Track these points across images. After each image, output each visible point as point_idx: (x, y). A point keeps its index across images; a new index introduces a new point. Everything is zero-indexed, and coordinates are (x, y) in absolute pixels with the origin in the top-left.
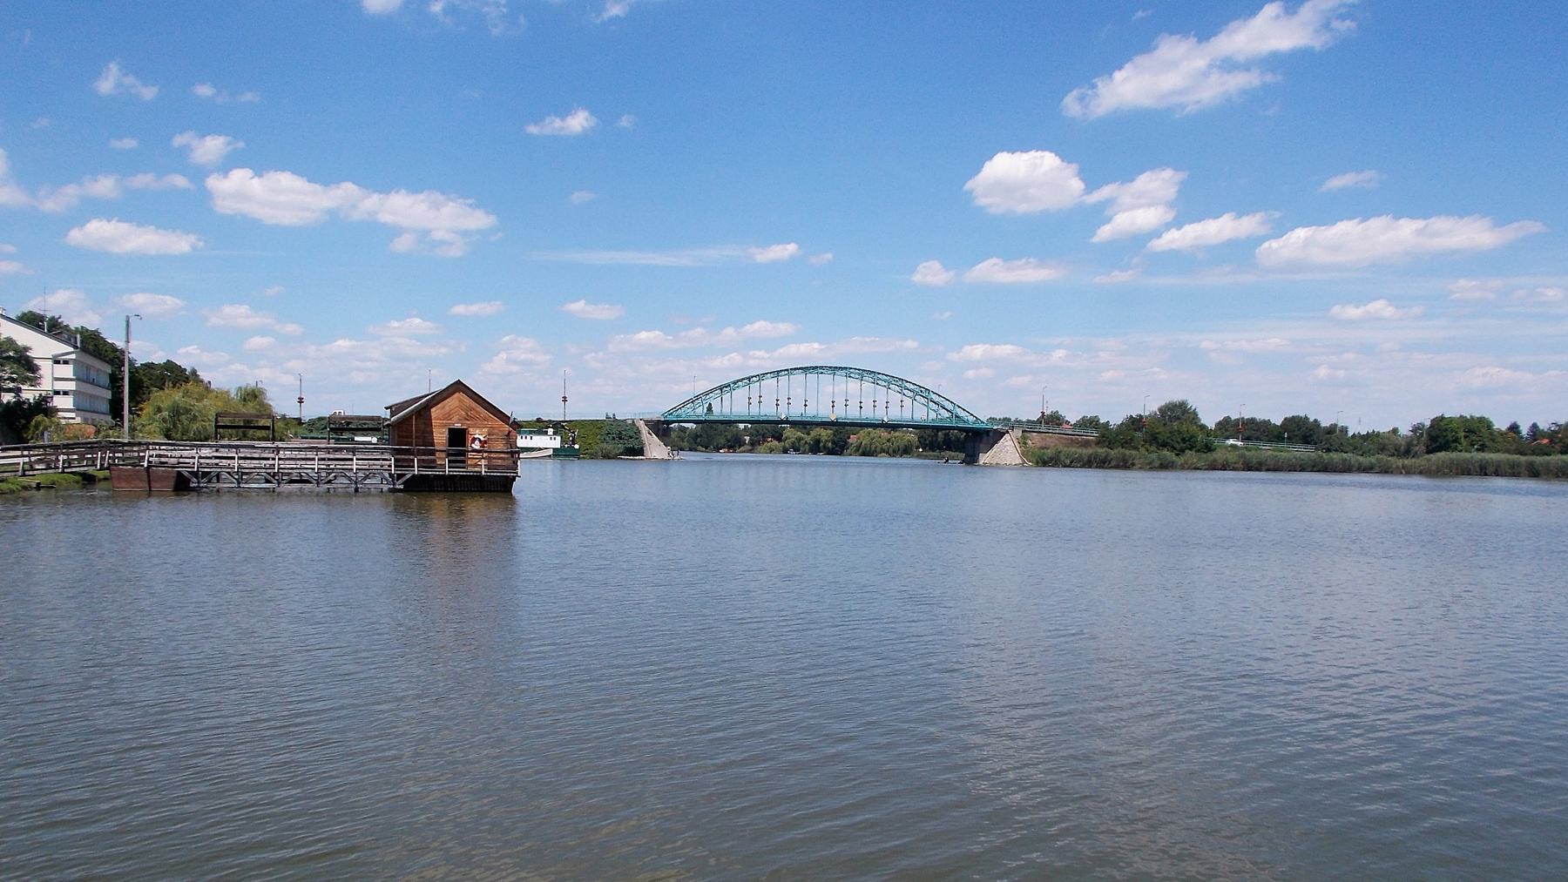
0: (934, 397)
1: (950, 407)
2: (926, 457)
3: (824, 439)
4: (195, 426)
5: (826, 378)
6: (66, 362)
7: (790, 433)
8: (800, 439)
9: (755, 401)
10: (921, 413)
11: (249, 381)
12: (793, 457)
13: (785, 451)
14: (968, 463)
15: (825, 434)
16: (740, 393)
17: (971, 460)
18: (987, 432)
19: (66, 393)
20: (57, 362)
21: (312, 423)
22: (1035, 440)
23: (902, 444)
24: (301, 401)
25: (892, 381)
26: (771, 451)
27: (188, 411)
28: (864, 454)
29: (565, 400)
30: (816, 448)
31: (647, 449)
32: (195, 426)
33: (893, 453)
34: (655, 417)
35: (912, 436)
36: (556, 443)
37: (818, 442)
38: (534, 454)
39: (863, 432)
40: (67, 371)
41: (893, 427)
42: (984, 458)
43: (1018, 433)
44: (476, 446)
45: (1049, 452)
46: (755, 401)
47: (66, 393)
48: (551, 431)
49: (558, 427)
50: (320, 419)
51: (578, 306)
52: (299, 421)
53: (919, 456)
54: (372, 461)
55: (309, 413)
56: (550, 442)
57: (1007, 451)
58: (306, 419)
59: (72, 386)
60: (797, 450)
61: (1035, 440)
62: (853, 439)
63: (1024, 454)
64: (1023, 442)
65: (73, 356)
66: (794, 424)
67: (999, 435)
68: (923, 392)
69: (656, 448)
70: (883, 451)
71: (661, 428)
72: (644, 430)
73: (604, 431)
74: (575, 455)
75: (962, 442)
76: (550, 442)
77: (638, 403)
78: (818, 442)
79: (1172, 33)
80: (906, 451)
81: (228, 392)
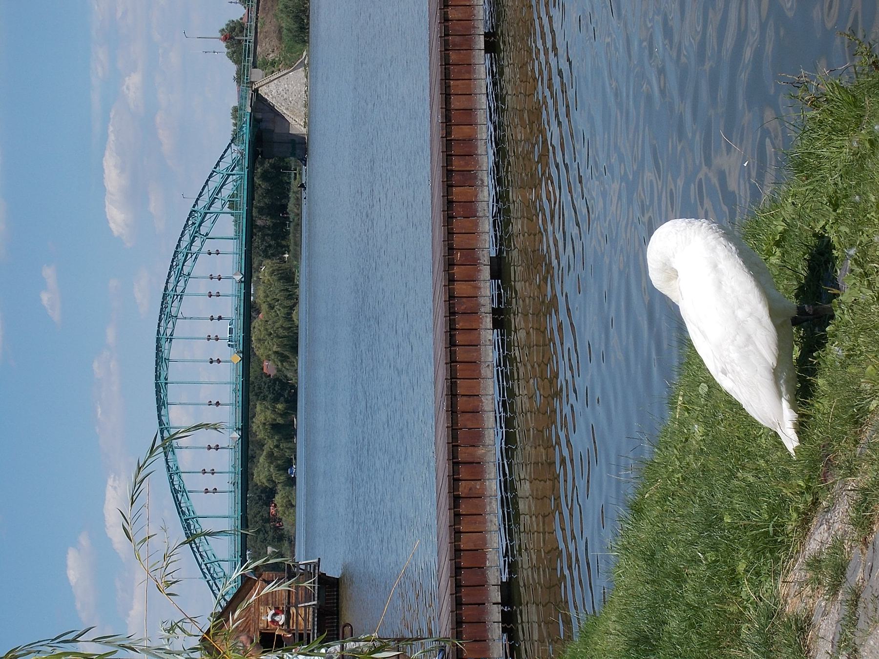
0: (202, 203)
1: (217, 180)
2: (298, 244)
5: (173, 372)
7: (262, 473)
8: (270, 455)
9: (211, 481)
10: (226, 228)
12: (299, 470)
13: (291, 482)
14: (305, 151)
15: (263, 415)
16: (198, 504)
17: (299, 147)
18: (256, 122)
22: (268, 48)
25: (177, 268)
26: (291, 505)
28: (294, 349)
30: (285, 430)
33: (292, 298)
35: (265, 270)
37: (275, 428)
39: (259, 351)
41: (249, 310)
42: (297, 127)
43: (257, 75)
44: (281, 619)
45: (287, 23)
46: (211, 481)
53: (297, 256)
57: (285, 91)
60: (289, 463)
61: (268, 48)
62: (270, 368)
63: (290, 65)
64: (270, 67)
66: (247, 459)
67: (260, 104)
68: (195, 223)
70: (288, 317)
78: (275, 428)
80: (288, 278)
81: (475, 73)
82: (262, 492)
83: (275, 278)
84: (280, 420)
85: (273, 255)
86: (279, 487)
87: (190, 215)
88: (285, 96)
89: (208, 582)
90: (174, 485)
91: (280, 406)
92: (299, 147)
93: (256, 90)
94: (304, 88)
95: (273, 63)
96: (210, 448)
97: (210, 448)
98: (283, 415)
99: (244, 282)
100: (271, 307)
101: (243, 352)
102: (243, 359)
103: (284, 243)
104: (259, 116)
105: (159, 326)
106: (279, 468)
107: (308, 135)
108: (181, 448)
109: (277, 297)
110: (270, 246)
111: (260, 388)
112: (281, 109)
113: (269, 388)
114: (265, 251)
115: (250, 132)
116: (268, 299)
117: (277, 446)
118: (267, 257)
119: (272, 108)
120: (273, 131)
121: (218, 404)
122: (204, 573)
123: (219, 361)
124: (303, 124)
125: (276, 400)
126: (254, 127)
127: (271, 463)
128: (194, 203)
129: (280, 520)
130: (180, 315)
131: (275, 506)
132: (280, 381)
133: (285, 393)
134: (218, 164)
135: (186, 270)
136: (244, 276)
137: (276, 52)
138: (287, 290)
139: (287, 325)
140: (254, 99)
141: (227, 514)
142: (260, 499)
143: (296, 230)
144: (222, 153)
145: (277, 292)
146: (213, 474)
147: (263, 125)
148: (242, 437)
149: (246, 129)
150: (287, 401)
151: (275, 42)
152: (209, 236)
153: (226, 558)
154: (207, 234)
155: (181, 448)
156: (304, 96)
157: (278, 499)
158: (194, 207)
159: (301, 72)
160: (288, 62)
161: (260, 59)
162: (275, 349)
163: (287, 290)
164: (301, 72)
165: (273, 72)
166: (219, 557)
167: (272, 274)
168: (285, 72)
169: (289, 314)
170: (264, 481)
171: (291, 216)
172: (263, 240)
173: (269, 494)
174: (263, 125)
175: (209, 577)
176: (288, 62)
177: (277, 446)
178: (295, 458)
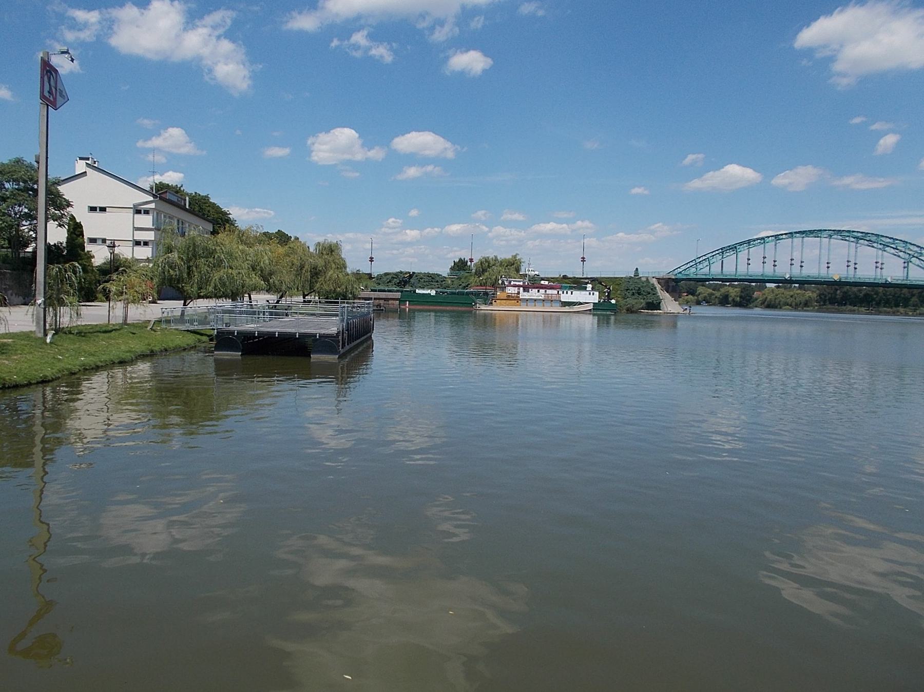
3: (733, 295)
4: (216, 276)
6: (147, 212)
11: (331, 238)
13: (698, 303)
16: (756, 252)
19: (146, 244)
20: (138, 212)
21: (380, 277)
23: (803, 299)
24: (371, 260)
27: (211, 253)
29: (583, 260)
30: (724, 301)
31: (663, 304)
32: (216, 276)
33: (796, 307)
35: (811, 294)
36: (595, 298)
38: (576, 308)
40: (146, 221)
47: (146, 244)
48: (589, 286)
49: (597, 282)
50: (386, 274)
52: (370, 276)
54: (367, 277)
55: (378, 269)
56: (590, 297)
58: (375, 275)
59: (150, 236)
65: (153, 206)
69: (670, 305)
72: (658, 287)
73: (623, 287)
74: (615, 309)
76: (590, 297)
77: (656, 265)
80: (806, 305)
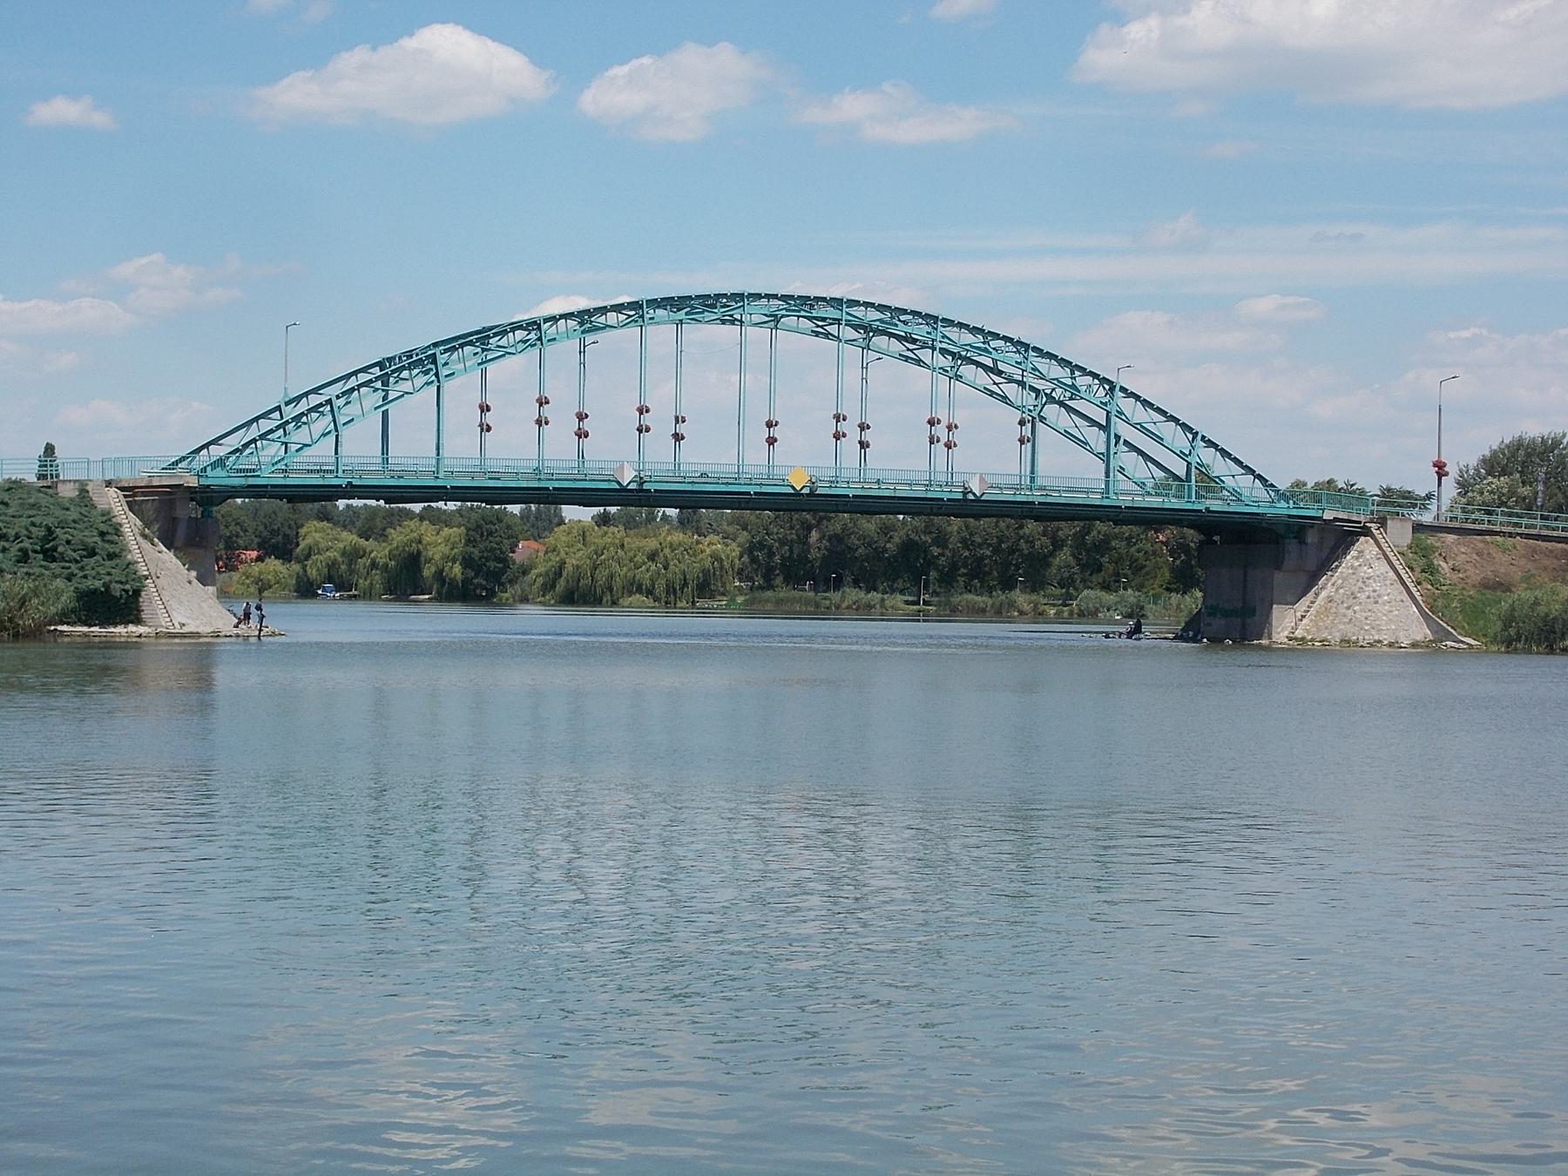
9: (661, 424)
13: (306, 590)
17: (1230, 624)
18: (1297, 529)
22: (1459, 559)
30: (406, 580)
31: (151, 601)
34: (140, 475)
35: (719, 545)
43: (1399, 533)
51: (853, 107)
57: (1367, 595)
63: (1433, 610)
64: (1421, 559)
67: (1342, 538)
69: (180, 600)
70: (634, 587)
71: (194, 516)
72: (130, 525)
75: (1228, 564)
79: (457, 24)
80: (702, 589)
82: (286, 536)
83: (708, 564)
84: (428, 571)
85: (754, 560)
86: (296, 567)
87: (1104, 380)
88: (1362, 596)
89: (278, 408)
90: (513, 330)
91: (457, 569)
92: (1230, 624)
93: (1366, 532)
94: (1386, 638)
95: (1429, 569)
96: (581, 417)
97: (581, 417)
98: (439, 576)
99: (965, 500)
100: (652, 557)
101: (812, 494)
102: (797, 494)
103: (779, 581)
104: (1311, 538)
105: (867, 305)
106: (332, 565)
107: (1268, 649)
108: (582, 352)
109: (671, 567)
110: (771, 554)
111: (490, 533)
112: (1328, 587)
113: (492, 550)
114: (761, 545)
115: (1277, 516)
116: (667, 551)
117: (374, 565)
118: (750, 550)
119: (1325, 565)
120: (1278, 567)
121: (678, 437)
122: (298, 399)
123: (771, 441)
124: (1299, 633)
125: (467, 562)
126: (1288, 526)
127: (344, 553)
128: (1131, 389)
129: (235, 569)
130: (872, 355)
131: (260, 559)
132: (503, 571)
133: (482, 580)
134: (1210, 444)
135: (967, 371)
136: (978, 500)
137: (1455, 577)
138: (685, 584)
139: (617, 584)
140: (1348, 527)
141: (445, 452)
142: (274, 533)
143: (807, 602)
144: (1234, 454)
145: (682, 566)
146: (539, 422)
147: (1292, 546)
148: (624, 489)
149: (1283, 508)
150: (466, 581)
151: (1475, 575)
152: (1039, 425)
153: (343, 450)
154: (1042, 419)
155: (582, 352)
156: (1369, 638)
157: (273, 564)
158: (1123, 389)
159: (1422, 632)
160: (1440, 603)
161: (1431, 541)
162: (571, 562)
163: (685, 584)
164: (1422, 632)
165: (1412, 569)
166: (345, 433)
167: (715, 557)
168: (1417, 595)
169: (639, 590)
170: (309, 541)
171: (835, 596)
172: (782, 542)
173: (280, 546)
174: (1292, 546)
175: (290, 412)
176: (1440, 603)
177: (374, 565)
178: (350, 597)
